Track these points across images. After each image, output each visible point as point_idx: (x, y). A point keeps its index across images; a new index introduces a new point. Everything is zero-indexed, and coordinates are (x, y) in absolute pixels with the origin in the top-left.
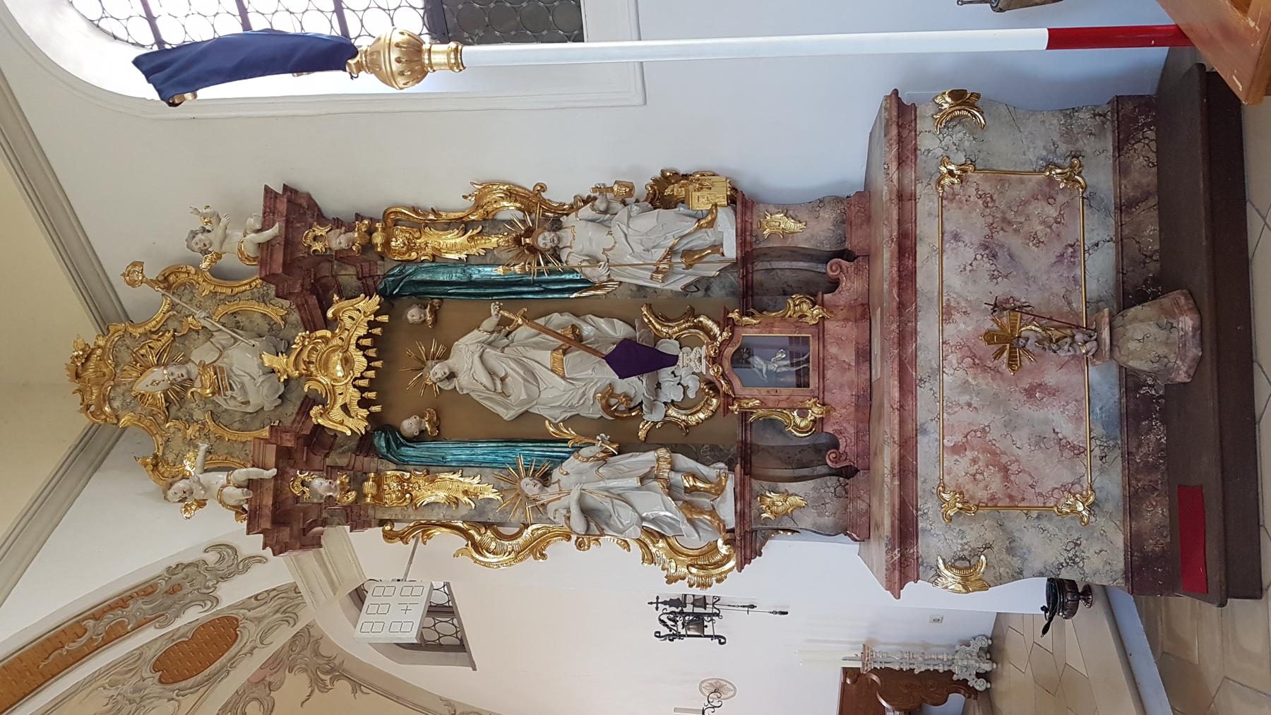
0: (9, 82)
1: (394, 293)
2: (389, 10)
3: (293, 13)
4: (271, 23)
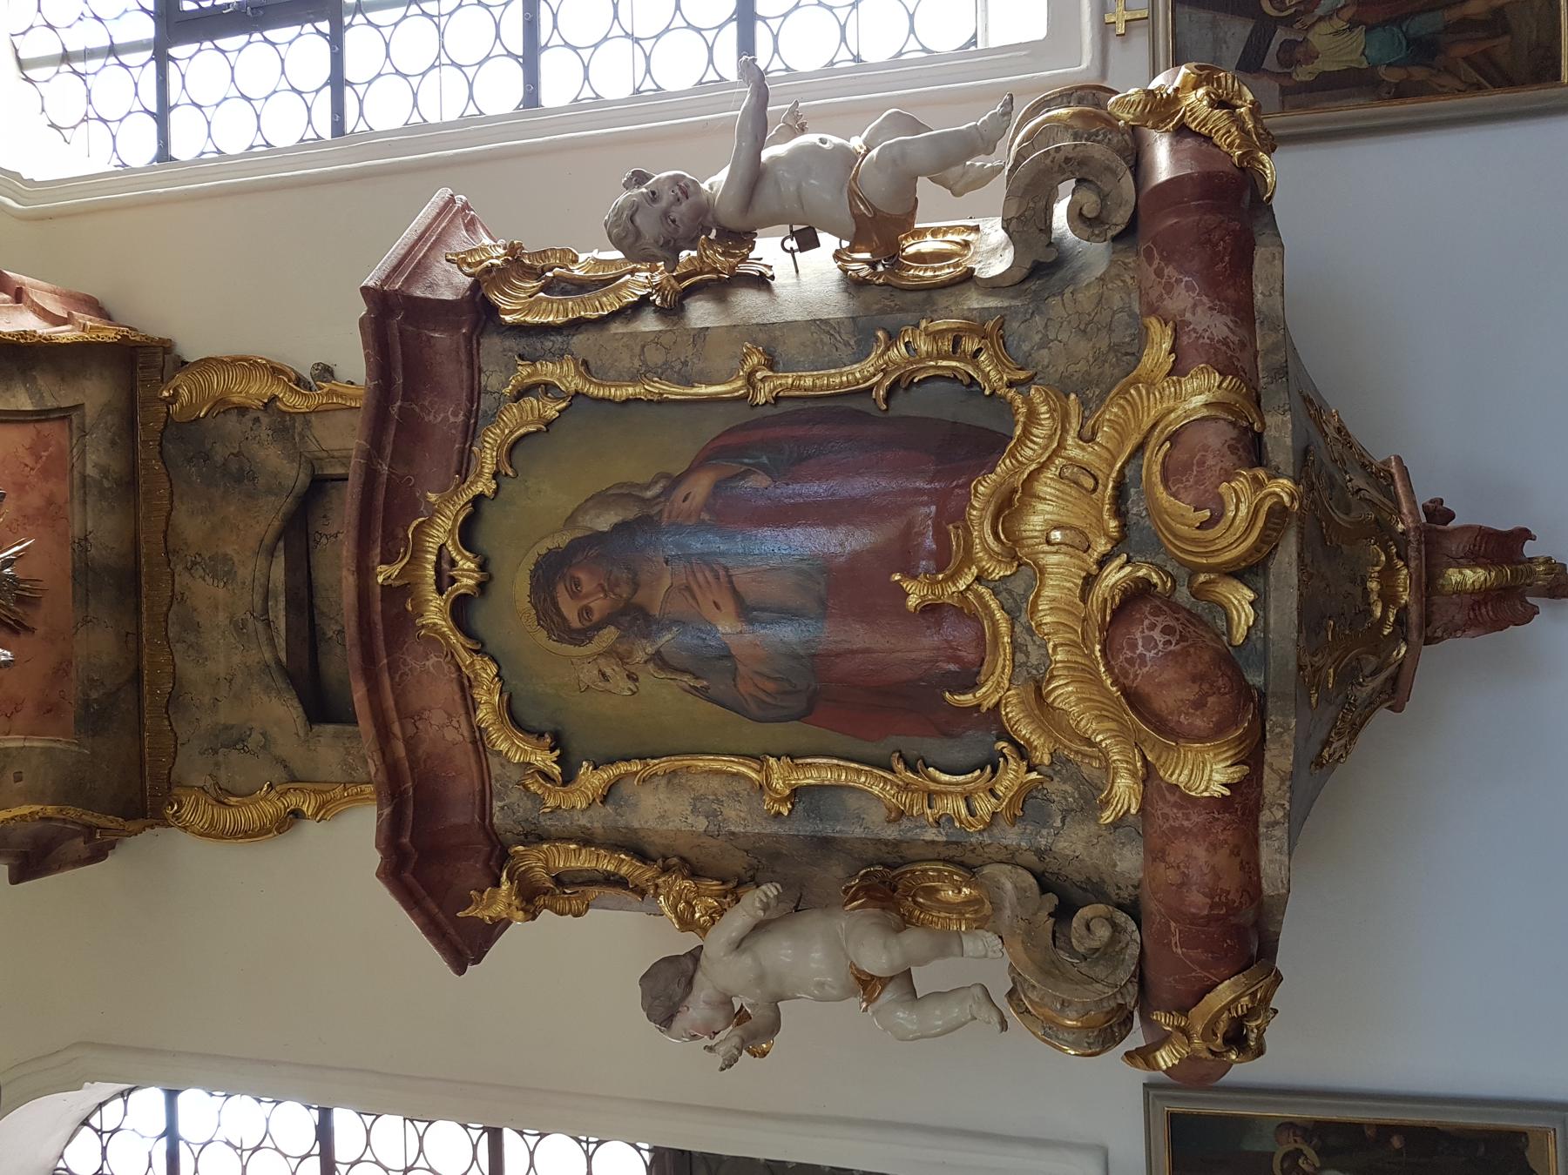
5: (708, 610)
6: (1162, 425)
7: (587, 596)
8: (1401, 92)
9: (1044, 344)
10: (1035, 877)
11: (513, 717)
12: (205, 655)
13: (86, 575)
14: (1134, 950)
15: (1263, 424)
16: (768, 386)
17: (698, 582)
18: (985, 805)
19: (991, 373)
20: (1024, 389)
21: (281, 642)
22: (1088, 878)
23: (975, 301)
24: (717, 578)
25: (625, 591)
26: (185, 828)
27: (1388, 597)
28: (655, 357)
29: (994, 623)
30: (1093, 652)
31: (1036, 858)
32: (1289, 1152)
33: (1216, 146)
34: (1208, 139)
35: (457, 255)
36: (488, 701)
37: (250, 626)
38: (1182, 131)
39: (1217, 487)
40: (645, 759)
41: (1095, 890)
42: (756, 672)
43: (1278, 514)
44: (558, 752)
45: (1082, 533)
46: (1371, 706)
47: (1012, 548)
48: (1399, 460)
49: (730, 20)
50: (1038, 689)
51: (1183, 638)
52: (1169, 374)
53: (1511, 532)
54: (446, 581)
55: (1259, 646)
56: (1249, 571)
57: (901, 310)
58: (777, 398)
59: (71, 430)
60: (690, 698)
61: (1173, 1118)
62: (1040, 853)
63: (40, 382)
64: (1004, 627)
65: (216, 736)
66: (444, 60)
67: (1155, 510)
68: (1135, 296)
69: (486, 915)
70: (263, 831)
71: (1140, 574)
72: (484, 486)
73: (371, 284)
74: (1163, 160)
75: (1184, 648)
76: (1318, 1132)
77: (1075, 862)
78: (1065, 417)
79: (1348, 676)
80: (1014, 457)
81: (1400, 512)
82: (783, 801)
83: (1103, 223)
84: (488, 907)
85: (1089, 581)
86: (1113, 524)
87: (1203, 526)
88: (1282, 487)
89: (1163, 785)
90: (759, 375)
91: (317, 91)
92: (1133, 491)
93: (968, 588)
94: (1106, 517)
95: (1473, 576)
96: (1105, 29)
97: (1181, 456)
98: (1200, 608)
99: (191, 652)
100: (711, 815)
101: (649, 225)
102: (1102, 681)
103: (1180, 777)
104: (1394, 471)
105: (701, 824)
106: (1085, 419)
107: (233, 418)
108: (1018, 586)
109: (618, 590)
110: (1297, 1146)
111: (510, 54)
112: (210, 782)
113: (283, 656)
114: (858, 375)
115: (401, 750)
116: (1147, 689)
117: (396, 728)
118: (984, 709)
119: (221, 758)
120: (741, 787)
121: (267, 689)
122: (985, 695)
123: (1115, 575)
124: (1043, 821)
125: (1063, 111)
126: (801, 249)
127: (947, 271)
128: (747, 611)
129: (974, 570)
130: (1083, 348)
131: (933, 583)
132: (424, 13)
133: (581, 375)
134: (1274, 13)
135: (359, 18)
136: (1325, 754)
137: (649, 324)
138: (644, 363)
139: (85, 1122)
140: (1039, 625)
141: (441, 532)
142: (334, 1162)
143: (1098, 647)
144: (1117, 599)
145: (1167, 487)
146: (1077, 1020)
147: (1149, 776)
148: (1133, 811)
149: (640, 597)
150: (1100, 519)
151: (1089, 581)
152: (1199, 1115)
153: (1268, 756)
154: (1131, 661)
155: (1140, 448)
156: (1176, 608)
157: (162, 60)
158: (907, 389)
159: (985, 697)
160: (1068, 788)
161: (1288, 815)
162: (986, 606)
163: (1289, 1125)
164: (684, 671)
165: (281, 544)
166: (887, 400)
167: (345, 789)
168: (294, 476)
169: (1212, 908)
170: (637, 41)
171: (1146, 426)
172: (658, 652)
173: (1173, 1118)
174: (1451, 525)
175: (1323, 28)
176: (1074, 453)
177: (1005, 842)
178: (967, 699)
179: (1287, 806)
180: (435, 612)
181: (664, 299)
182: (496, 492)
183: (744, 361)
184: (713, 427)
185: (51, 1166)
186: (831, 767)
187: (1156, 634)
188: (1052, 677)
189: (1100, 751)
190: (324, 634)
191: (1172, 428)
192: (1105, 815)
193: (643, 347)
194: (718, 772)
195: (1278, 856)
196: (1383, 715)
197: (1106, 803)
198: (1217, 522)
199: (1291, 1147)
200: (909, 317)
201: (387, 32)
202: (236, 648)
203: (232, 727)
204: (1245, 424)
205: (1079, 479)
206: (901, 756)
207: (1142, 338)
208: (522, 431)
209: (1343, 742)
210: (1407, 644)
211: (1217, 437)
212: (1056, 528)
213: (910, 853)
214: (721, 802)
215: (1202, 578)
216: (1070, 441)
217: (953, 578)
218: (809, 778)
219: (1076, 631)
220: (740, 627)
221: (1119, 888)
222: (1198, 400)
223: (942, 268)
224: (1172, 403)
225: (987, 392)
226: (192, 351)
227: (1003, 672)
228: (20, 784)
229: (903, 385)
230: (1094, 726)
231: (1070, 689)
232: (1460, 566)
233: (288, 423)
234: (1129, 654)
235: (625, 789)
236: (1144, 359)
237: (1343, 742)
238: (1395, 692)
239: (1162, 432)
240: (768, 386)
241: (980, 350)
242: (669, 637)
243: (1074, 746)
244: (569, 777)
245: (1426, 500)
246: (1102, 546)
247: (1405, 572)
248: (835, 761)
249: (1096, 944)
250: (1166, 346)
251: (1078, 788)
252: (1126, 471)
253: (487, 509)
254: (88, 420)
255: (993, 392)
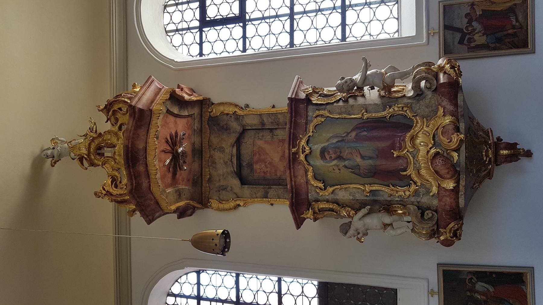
0: (535, 282)
1: (468, 25)
2: (216, 287)
3: (259, 279)
4: (337, 27)
5: (355, 157)
6: (441, 125)
7: (331, 154)
8: (494, 49)
9: (419, 109)
10: (417, 207)
11: (315, 178)
12: (217, 169)
13: (194, 150)
14: (436, 218)
15: (459, 125)
16: (366, 116)
17: (353, 152)
18: (407, 193)
19: (409, 114)
20: (415, 117)
21: (235, 166)
22: (427, 207)
23: (405, 101)
24: (357, 151)
25: (338, 154)
26: (212, 208)
27: (487, 156)
28: (343, 110)
29: (410, 159)
30: (429, 164)
31: (417, 203)
32: (470, 278)
33: (451, 76)
34: (450, 75)
35: (303, 90)
36: (310, 174)
37: (228, 163)
38: (445, 73)
39: (451, 136)
40: (341, 185)
41: (429, 208)
42: (364, 169)
43: (461, 140)
44: (324, 184)
45: (427, 143)
46: (484, 177)
47: (414, 146)
48: (490, 129)
49: (340, 25)
50: (418, 171)
51: (445, 162)
52: (443, 116)
53: (513, 143)
54: (303, 152)
55: (459, 163)
56: (457, 150)
57: (392, 102)
58: (368, 118)
59: (192, 119)
60: (351, 173)
61: (444, 271)
62: (418, 202)
63: (189, 109)
64: (412, 160)
65: (220, 188)
66: (271, 33)
67: (440, 140)
68: (436, 101)
69: (305, 217)
70: (230, 209)
71: (438, 150)
72: (311, 134)
73: (290, 97)
74: (442, 78)
75: (445, 163)
76: (476, 273)
77: (425, 203)
78: (424, 122)
79: (479, 171)
80: (414, 129)
81: (490, 139)
82: (368, 193)
83: (431, 88)
84: (306, 215)
85: (428, 152)
86: (433, 142)
87: (449, 142)
88: (462, 136)
89: (442, 187)
90: (364, 114)
91: (239, 39)
92: (436, 136)
93: (405, 153)
94: (431, 140)
95: (505, 152)
96: (428, 34)
97: (445, 130)
98: (448, 157)
99: (214, 169)
100: (353, 196)
101: (345, 88)
102: (431, 169)
103: (445, 186)
104: (489, 131)
105: (351, 198)
106: (427, 123)
107: (225, 116)
108: (415, 153)
109: (337, 153)
110: (472, 277)
111: (286, 32)
112: (218, 198)
113: (235, 170)
114: (383, 114)
115: (293, 183)
116: (439, 170)
117: (293, 179)
118: (408, 175)
119: (220, 192)
120: (359, 190)
121: (232, 177)
122: (408, 172)
123: (433, 151)
124: (419, 196)
125: (423, 68)
126: (371, 90)
127: (400, 95)
128: (363, 157)
129: (407, 150)
130: (427, 110)
131: (399, 152)
132: (266, 22)
133: (329, 113)
134: (466, 32)
135: (250, 23)
136: (474, 186)
137: (341, 103)
138: (341, 111)
139: (177, 281)
140: (419, 160)
141: (303, 143)
142: (239, 289)
143: (430, 163)
144: (433, 155)
145: (442, 136)
146: (425, 232)
147: (439, 186)
148: (436, 193)
149: (341, 155)
150: (430, 141)
151: (428, 152)
152: (450, 270)
153: (460, 182)
154: (436, 166)
155: (437, 129)
156: (444, 156)
157: (201, 31)
158: (393, 117)
159: (408, 173)
160: (424, 190)
161: (464, 193)
162: (409, 156)
163: (470, 272)
164: (350, 168)
165: (235, 144)
166: (389, 119)
167: (251, 200)
168: (239, 129)
169: (450, 208)
170: (317, 29)
171: (438, 125)
172: (345, 165)
173: (444, 271)
174: (502, 142)
175: (477, 35)
176: (425, 129)
177: (411, 200)
178: (405, 173)
179: (464, 191)
180: (302, 157)
181: (345, 99)
182: (313, 135)
183: (361, 111)
184: (355, 123)
185: (168, 291)
186: (377, 186)
187: (440, 161)
188: (421, 169)
189: (430, 182)
190: (243, 165)
191: (443, 125)
192: (431, 194)
193: (341, 108)
194: (355, 188)
195: (462, 201)
196: (487, 181)
197: (431, 192)
198: (450, 142)
199: (470, 277)
200: (394, 104)
201: (256, 26)
202: (225, 168)
203: (223, 186)
204: (456, 125)
205: (426, 134)
206: (391, 184)
207: (438, 109)
208: (317, 123)
209: (478, 184)
210: (491, 165)
211: (451, 127)
212: (422, 142)
213: (392, 203)
214: (355, 194)
215: (449, 151)
216: (424, 127)
217: (403, 151)
218: (374, 188)
219: (426, 161)
220: (361, 160)
221: (433, 207)
222: (448, 121)
223: (399, 94)
224: (443, 121)
225: (408, 117)
226: (215, 100)
227: (412, 168)
228: (185, 196)
229: (392, 116)
230: (429, 178)
231: (425, 171)
232: (503, 150)
233: (238, 117)
234: (436, 164)
235: (336, 191)
236: (438, 113)
237: (478, 184)
238: (490, 175)
239: (441, 126)
240: (366, 116)
241: (407, 110)
242: (347, 162)
243: (425, 182)
244: (325, 189)
245: (497, 137)
246: (430, 146)
247: (491, 151)
248: (379, 185)
249: (429, 217)
250: (442, 111)
251: (425, 190)
252: (435, 132)
253: (311, 138)
254: (195, 117)
255: (410, 117)
